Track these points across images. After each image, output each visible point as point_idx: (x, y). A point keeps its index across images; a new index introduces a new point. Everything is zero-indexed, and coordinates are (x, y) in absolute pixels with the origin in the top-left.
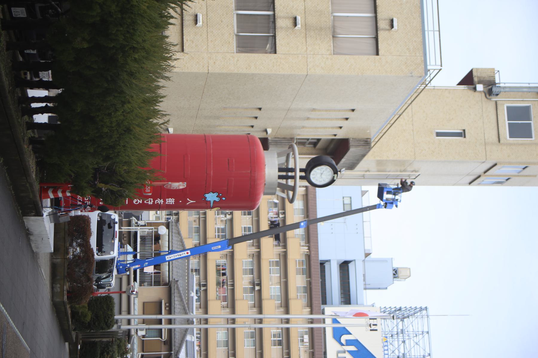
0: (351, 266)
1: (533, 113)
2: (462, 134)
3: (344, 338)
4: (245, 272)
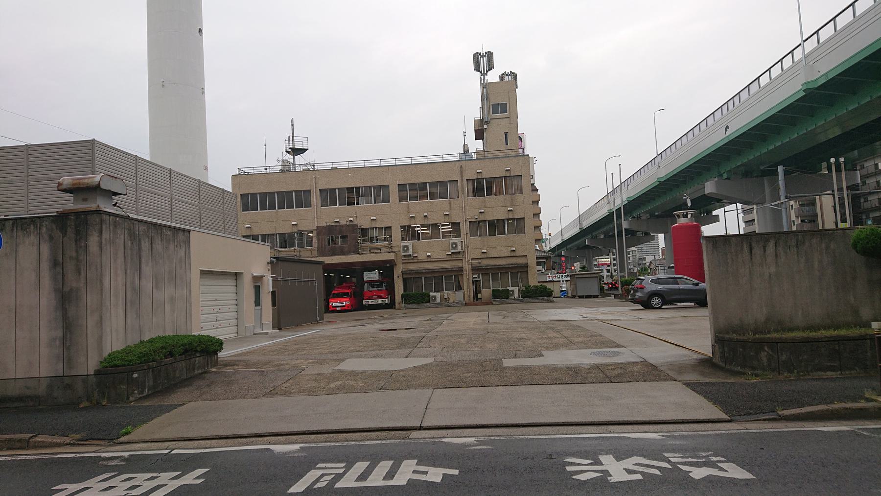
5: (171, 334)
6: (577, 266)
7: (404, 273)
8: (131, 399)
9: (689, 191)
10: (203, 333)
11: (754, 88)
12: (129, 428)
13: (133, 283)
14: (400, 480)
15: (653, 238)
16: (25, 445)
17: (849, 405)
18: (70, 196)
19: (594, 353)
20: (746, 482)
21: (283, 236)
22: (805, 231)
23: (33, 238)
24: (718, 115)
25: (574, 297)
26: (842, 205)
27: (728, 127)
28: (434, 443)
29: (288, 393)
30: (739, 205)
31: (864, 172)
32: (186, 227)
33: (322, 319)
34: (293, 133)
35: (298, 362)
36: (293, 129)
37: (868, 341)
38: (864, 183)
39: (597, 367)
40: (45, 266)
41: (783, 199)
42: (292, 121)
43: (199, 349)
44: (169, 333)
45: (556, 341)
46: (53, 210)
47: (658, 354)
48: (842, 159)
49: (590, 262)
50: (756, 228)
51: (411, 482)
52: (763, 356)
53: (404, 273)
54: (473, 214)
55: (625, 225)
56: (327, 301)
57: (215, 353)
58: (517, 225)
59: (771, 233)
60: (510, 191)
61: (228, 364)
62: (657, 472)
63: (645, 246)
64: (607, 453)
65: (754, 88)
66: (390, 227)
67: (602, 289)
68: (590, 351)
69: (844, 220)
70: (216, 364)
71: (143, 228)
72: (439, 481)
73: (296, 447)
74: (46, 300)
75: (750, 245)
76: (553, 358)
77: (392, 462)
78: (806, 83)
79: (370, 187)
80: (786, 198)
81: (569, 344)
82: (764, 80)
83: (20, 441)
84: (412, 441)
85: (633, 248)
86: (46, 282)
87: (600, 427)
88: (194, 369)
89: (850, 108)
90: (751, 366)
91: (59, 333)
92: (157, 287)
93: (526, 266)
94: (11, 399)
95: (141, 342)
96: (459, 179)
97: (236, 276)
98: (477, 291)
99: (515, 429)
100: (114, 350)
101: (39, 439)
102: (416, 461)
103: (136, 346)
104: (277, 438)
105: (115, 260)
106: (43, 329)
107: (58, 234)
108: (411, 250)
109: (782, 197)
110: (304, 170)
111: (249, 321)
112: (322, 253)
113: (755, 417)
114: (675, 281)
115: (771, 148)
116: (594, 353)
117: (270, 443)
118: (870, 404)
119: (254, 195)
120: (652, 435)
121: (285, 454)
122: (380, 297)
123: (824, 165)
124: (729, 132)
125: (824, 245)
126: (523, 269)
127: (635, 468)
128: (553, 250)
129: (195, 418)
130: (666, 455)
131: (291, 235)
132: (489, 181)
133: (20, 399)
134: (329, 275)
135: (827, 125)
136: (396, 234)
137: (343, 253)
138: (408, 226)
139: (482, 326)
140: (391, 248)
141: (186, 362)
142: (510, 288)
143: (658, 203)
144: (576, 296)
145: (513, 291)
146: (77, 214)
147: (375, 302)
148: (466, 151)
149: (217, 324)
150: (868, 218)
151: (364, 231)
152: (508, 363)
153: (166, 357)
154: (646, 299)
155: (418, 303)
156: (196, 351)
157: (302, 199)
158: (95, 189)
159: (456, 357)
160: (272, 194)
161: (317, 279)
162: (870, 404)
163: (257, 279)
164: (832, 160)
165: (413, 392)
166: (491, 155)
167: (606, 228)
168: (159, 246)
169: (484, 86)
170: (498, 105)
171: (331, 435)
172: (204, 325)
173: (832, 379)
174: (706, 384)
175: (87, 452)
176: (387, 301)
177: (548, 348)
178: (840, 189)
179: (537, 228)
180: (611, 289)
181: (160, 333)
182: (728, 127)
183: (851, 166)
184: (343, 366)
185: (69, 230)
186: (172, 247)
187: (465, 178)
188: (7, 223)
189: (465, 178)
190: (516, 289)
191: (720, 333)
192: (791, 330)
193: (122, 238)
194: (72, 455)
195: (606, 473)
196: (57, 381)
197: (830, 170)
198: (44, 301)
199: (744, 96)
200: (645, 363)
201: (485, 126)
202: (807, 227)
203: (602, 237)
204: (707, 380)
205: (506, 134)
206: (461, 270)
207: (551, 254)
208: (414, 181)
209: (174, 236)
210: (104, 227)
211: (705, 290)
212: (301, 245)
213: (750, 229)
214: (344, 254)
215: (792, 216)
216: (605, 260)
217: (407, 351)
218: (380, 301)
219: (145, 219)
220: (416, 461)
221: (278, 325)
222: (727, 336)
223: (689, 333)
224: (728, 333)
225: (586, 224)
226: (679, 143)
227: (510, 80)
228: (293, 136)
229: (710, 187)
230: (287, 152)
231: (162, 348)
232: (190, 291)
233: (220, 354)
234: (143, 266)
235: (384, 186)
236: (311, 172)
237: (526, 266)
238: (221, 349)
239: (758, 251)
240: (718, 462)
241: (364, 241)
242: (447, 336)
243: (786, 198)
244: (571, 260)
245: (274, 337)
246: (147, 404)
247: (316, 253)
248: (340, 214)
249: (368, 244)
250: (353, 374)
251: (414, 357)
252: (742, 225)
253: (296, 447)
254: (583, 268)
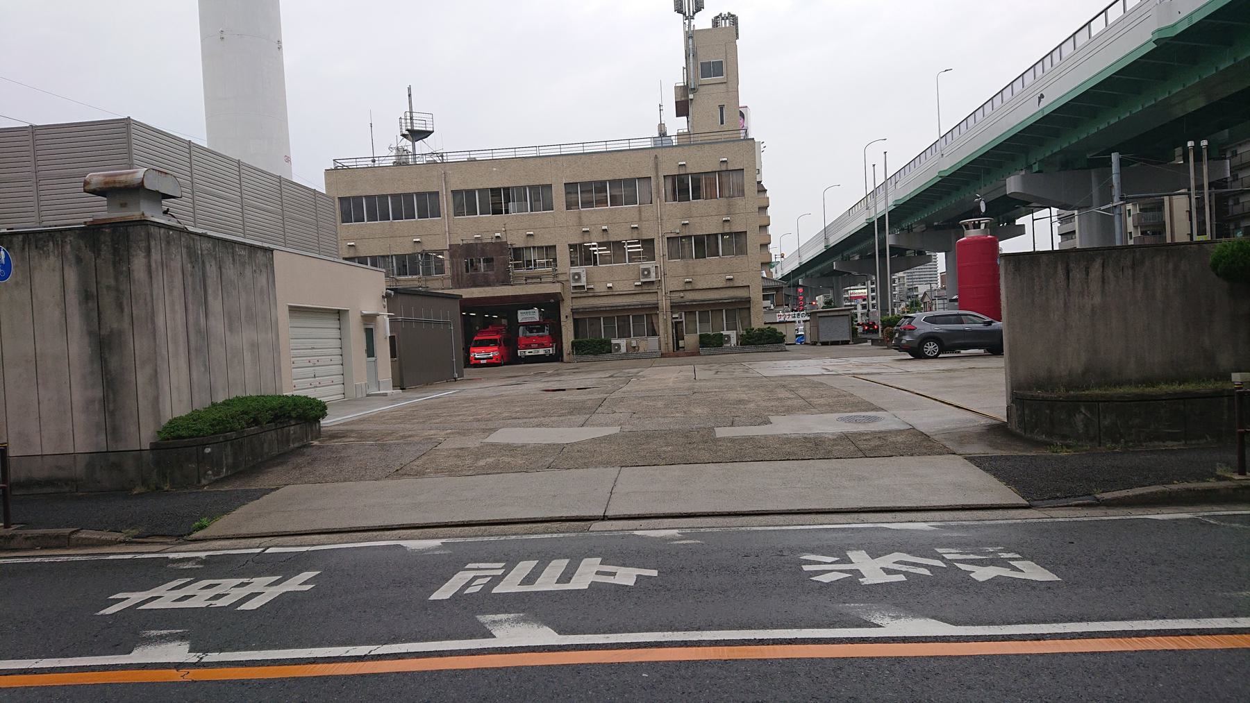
5: (254, 394)
6: (820, 300)
7: (574, 311)
8: (204, 482)
9: (983, 191)
10: (296, 393)
11: (1082, 38)
12: (204, 521)
13: (197, 323)
14: (580, 582)
15: (929, 259)
16: (65, 542)
17: (1193, 485)
18: (103, 200)
19: (842, 419)
20: (1049, 585)
21: (401, 258)
22: (1145, 246)
23: (53, 261)
24: (1029, 78)
25: (814, 344)
26: (1201, 210)
27: (1042, 96)
28: (623, 537)
29: (420, 474)
30: (1055, 211)
31: (1237, 161)
32: (266, 245)
33: (461, 375)
34: (411, 107)
35: (432, 432)
36: (410, 102)
37: (1226, 399)
38: (1235, 177)
39: (845, 437)
40: (73, 299)
41: (1116, 201)
42: (409, 89)
43: (293, 414)
44: (251, 392)
45: (789, 403)
46: (80, 220)
47: (931, 419)
48: (1204, 143)
49: (838, 295)
50: (1077, 243)
51: (593, 585)
52: (1079, 418)
53: (574, 311)
54: (673, 227)
55: (890, 240)
56: (467, 351)
57: (316, 420)
58: (736, 241)
59: (1097, 249)
60: (726, 193)
61: (334, 436)
62: (927, 572)
63: (917, 271)
64: (858, 547)
65: (1082, 38)
66: (555, 247)
67: (854, 331)
68: (837, 415)
69: (1202, 232)
70: (318, 434)
71: (207, 245)
72: (631, 583)
73: (438, 542)
74: (77, 347)
75: (1068, 266)
76: (784, 426)
77: (567, 561)
78: (1159, 30)
79: (525, 188)
80: (1121, 199)
81: (808, 407)
82: (1098, 26)
83: (57, 537)
84: (594, 534)
85: (901, 274)
86: (76, 321)
87: (849, 516)
88: (288, 441)
89: (1222, 67)
90: (1062, 437)
91: (99, 393)
92: (231, 330)
93: (748, 300)
94: (39, 483)
95: (214, 405)
96: (652, 175)
97: (339, 314)
98: (678, 336)
99: (733, 519)
100: (176, 415)
101: (83, 534)
102: (600, 559)
103: (207, 410)
104: (409, 531)
105: (171, 291)
106: (78, 389)
107: (88, 255)
108: (584, 279)
109: (1116, 199)
110: (429, 163)
111: (360, 377)
112: (458, 283)
113: (1063, 502)
114: (958, 319)
115: (1065, 145)
116: (842, 419)
117: (400, 538)
118: (1222, 484)
119: (358, 199)
120: (920, 525)
121: (421, 551)
122: (541, 346)
123: (1179, 151)
124: (1044, 103)
125: (1171, 266)
126: (741, 306)
127: (897, 567)
128: (784, 278)
129: (295, 504)
130: (939, 550)
131: (413, 257)
132: (697, 178)
133: (50, 482)
134: (468, 315)
135: (1185, 93)
136: (563, 255)
137: (487, 283)
138: (580, 245)
139: (687, 385)
140: (556, 276)
141: (276, 433)
142: (725, 333)
143: (937, 208)
144: (818, 342)
145: (729, 336)
146: (115, 225)
147: (534, 352)
148: (663, 134)
149: (316, 381)
150: (1237, 228)
151: (517, 252)
152: (721, 432)
153: (249, 425)
154: (916, 345)
155: (595, 354)
156: (290, 417)
157: (427, 204)
158: (138, 190)
159: (649, 425)
160: (383, 198)
161: (453, 315)
162: (1222, 484)
163: (369, 319)
164: (1190, 144)
165: (592, 471)
166: (700, 139)
167: (862, 246)
168: (230, 271)
169: (690, 35)
170: (710, 64)
171: (483, 528)
172: (297, 383)
173: (1172, 452)
174: (995, 458)
175: (149, 552)
176: (551, 351)
177: (777, 413)
178: (1199, 187)
179: (765, 246)
180: (868, 332)
181: (239, 393)
182: (1042, 96)
183: (1217, 153)
184: (495, 438)
185: (104, 247)
186: (248, 272)
187: (661, 175)
188: (15, 239)
189: (661, 175)
190: (733, 334)
191: (1019, 389)
192: (1119, 384)
193: (178, 259)
194: (130, 556)
195: (857, 573)
196: (97, 458)
197: (1186, 159)
198: (74, 349)
199: (1068, 49)
200: (913, 431)
201: (691, 96)
202: (1149, 240)
203: (857, 258)
204: (998, 453)
205: (721, 108)
206: (656, 307)
207: (784, 284)
208: (587, 179)
209: (250, 257)
210: (153, 243)
211: (1001, 331)
212: (427, 272)
213: (1069, 245)
214: (489, 285)
215: (1129, 224)
216: (862, 291)
217: (582, 419)
218: (541, 352)
219: (210, 233)
220: (600, 559)
221: (401, 383)
222: (1029, 393)
223: (978, 390)
224: (1030, 389)
225: (834, 240)
226: (956, 131)
227: (728, 25)
228: (411, 112)
229: (1013, 185)
230: (404, 136)
231: (244, 413)
232: (277, 335)
233: (323, 422)
234: (210, 298)
235: (543, 186)
236: (439, 165)
237: (748, 300)
238: (324, 415)
239: (1077, 274)
240: (1010, 559)
241: (517, 266)
242: (637, 398)
243: (1121, 199)
244: (811, 292)
245: (395, 400)
246: (226, 488)
247: (449, 283)
248: (482, 227)
249: (523, 271)
250: (510, 449)
251: (593, 425)
252: (1057, 239)
253: (438, 542)
254: (828, 303)
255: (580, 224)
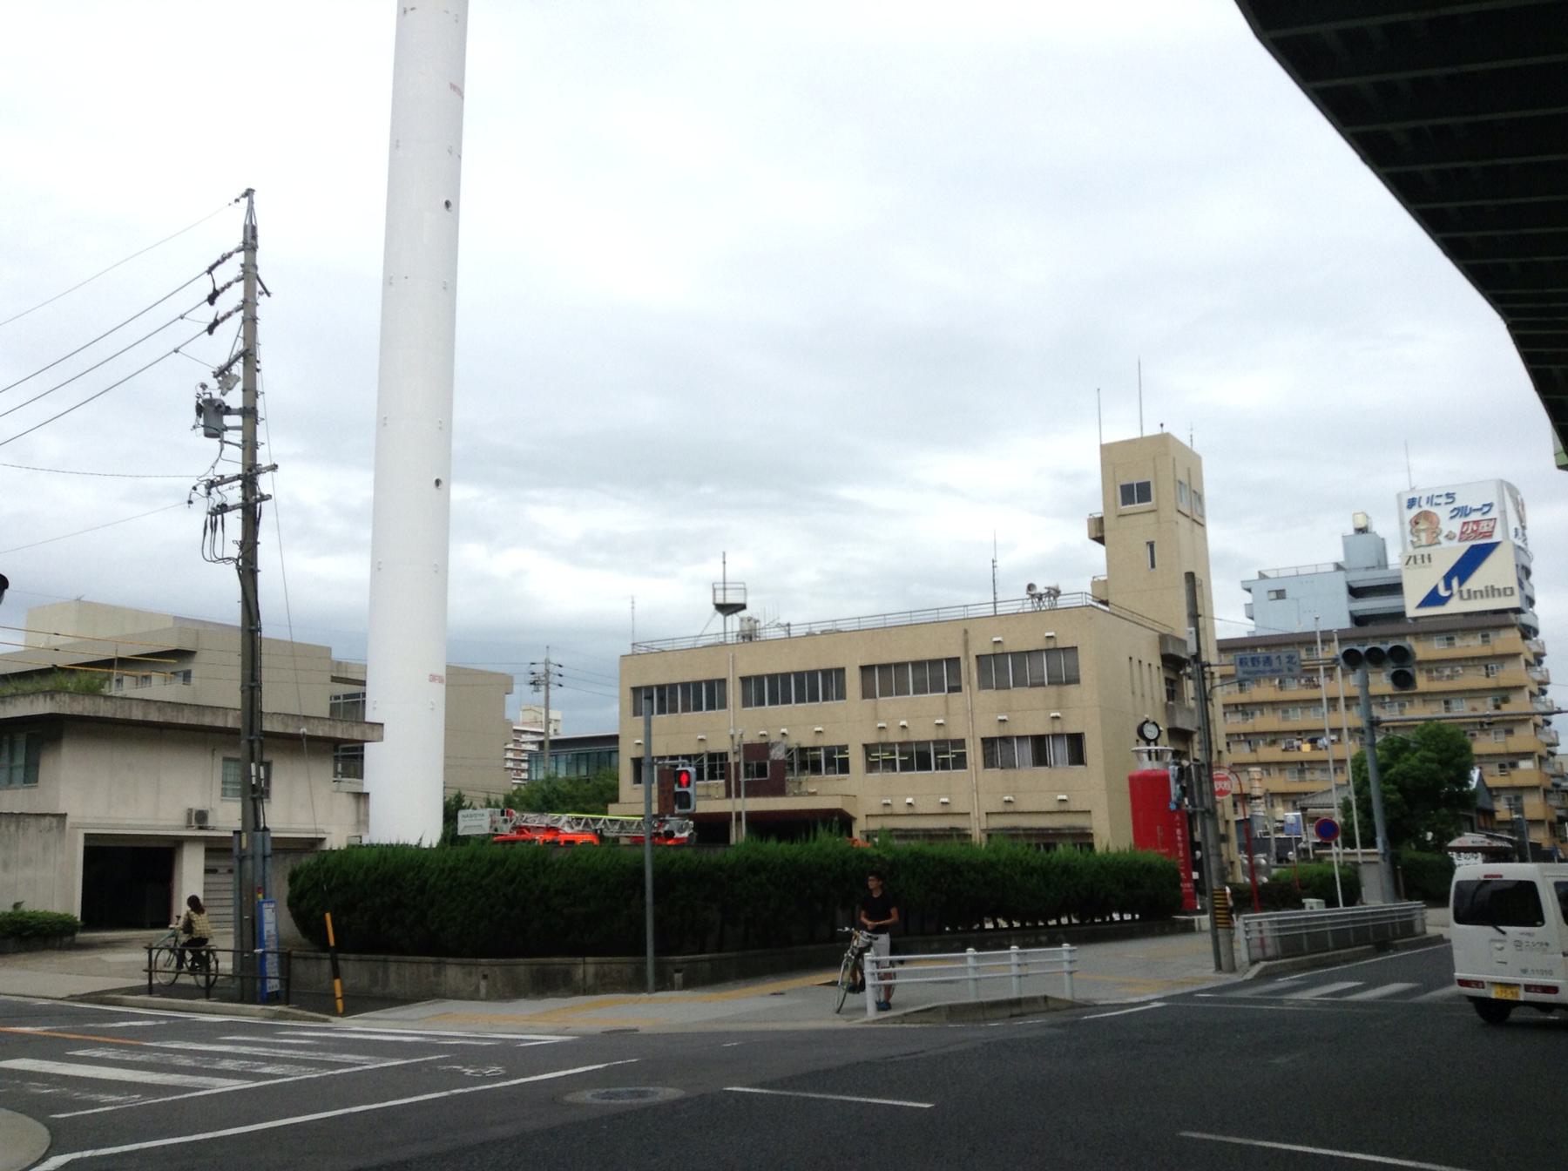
0: (1355, 585)
1: (1126, 482)
2: (1151, 545)
3: (1443, 592)
4: (1253, 751)
208: (688, 679)
255: (877, 718)
